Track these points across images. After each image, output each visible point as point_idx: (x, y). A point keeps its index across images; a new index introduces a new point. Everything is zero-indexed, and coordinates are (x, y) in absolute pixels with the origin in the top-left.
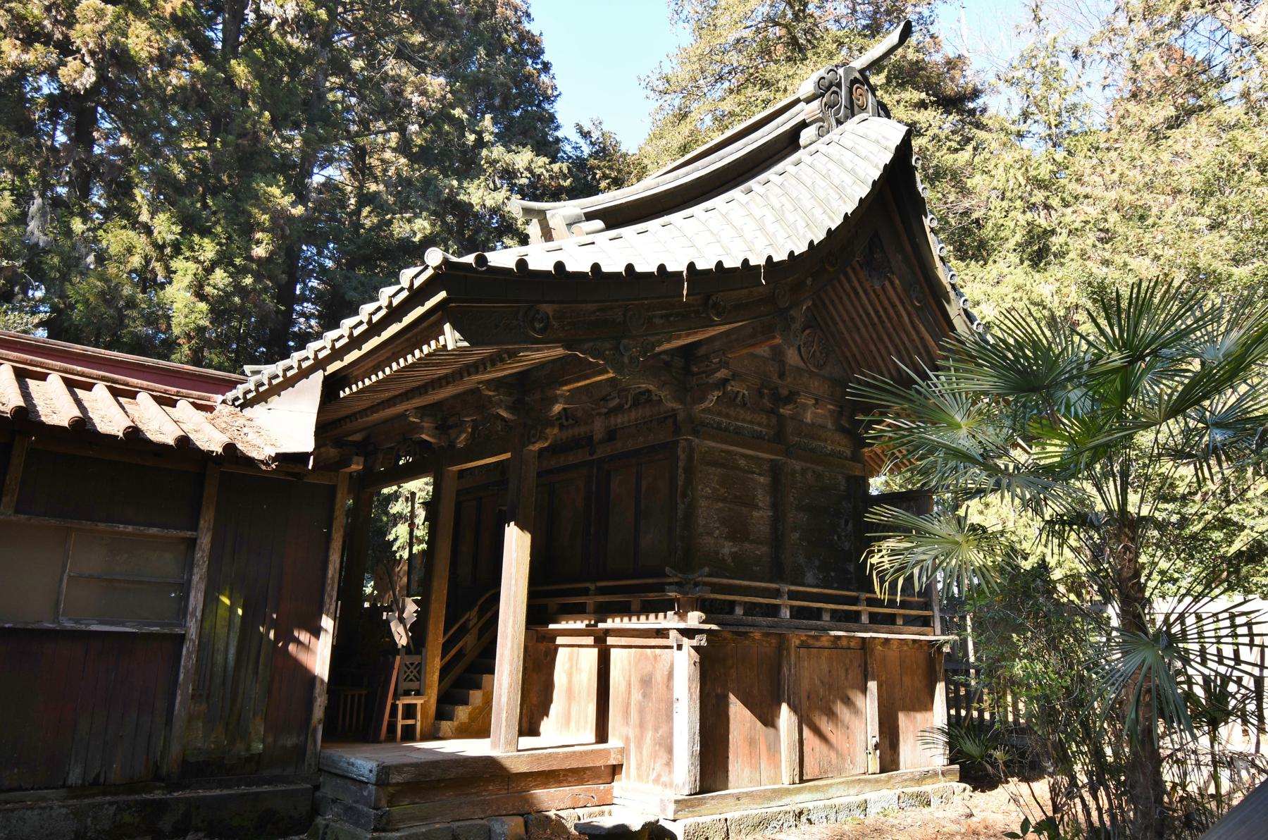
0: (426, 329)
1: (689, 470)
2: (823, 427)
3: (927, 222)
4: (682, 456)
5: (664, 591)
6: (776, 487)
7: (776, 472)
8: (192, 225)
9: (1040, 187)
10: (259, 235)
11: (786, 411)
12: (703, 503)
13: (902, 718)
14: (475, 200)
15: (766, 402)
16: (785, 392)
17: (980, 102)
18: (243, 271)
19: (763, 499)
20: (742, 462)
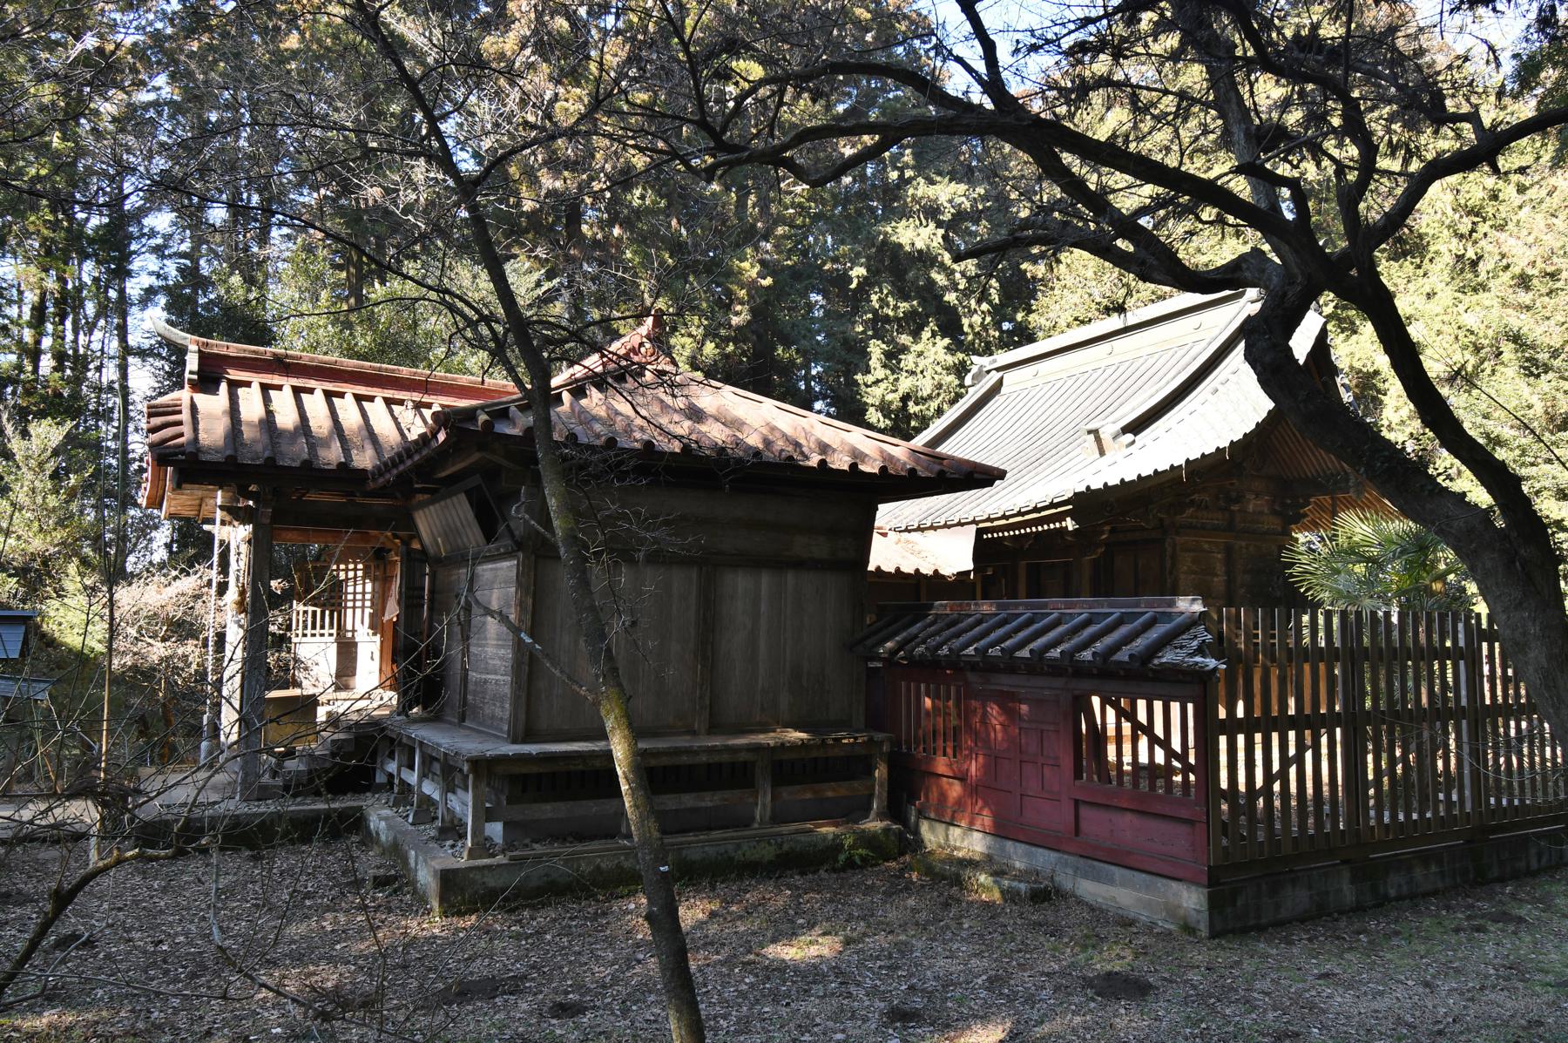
0: (1060, 517)
1: (1174, 557)
2: (1261, 513)
3: (1338, 380)
4: (1169, 549)
5: (985, 547)
6: (1229, 561)
7: (1229, 551)
8: (685, 306)
9: (1468, 214)
10: (739, 308)
11: (1235, 508)
12: (1182, 576)
13: (694, 573)
14: (903, 241)
15: (1222, 503)
16: (1234, 494)
17: (1427, 59)
18: (726, 340)
19: (1220, 568)
20: (1206, 546)
